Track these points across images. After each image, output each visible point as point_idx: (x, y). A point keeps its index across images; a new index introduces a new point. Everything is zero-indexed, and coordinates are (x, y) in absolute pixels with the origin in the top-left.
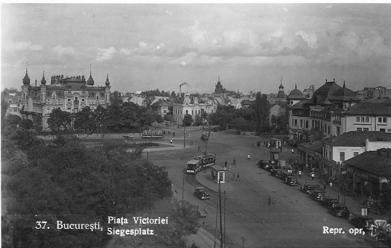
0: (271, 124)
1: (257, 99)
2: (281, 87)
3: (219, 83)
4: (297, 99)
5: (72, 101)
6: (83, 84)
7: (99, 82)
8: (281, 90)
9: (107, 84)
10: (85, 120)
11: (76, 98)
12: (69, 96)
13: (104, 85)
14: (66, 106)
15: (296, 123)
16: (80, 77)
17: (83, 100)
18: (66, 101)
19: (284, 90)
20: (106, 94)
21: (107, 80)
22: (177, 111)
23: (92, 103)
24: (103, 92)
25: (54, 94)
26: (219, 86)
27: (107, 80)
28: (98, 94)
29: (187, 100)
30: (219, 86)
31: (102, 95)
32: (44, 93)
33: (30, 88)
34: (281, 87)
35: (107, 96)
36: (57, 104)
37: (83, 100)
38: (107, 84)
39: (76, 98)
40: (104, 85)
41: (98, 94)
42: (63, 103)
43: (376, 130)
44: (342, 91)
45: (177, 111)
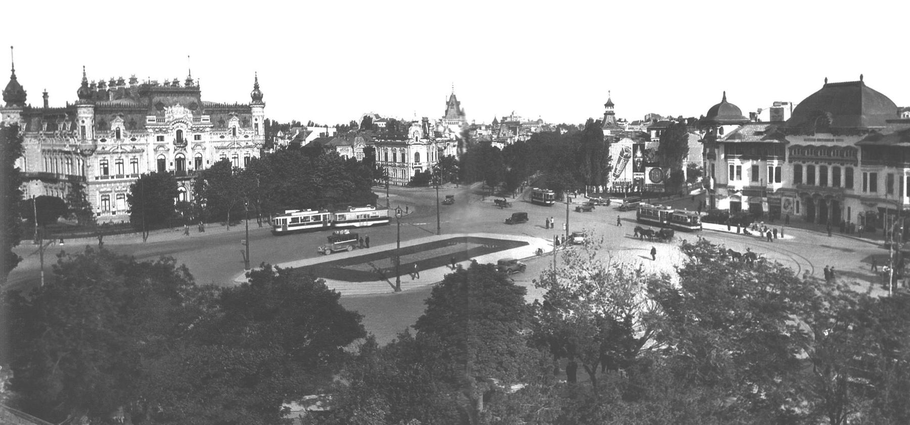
2: (609, 104)
4: (731, 124)
5: (170, 138)
6: (514, 126)
8: (609, 109)
9: (257, 97)
10: (228, 193)
11: (179, 133)
12: (161, 130)
14: (151, 152)
15: (739, 173)
16: (121, 81)
17: (198, 137)
18: (152, 139)
19: (615, 110)
20: (254, 121)
21: (256, 87)
23: (209, 149)
24: (247, 115)
25: (117, 124)
26: (453, 103)
27: (256, 87)
31: (245, 123)
32: (88, 124)
33: (28, 113)
34: (609, 104)
35: (256, 125)
36: (129, 148)
37: (198, 137)
38: (257, 97)
39: (179, 133)
40: (247, 100)
41: (234, 123)
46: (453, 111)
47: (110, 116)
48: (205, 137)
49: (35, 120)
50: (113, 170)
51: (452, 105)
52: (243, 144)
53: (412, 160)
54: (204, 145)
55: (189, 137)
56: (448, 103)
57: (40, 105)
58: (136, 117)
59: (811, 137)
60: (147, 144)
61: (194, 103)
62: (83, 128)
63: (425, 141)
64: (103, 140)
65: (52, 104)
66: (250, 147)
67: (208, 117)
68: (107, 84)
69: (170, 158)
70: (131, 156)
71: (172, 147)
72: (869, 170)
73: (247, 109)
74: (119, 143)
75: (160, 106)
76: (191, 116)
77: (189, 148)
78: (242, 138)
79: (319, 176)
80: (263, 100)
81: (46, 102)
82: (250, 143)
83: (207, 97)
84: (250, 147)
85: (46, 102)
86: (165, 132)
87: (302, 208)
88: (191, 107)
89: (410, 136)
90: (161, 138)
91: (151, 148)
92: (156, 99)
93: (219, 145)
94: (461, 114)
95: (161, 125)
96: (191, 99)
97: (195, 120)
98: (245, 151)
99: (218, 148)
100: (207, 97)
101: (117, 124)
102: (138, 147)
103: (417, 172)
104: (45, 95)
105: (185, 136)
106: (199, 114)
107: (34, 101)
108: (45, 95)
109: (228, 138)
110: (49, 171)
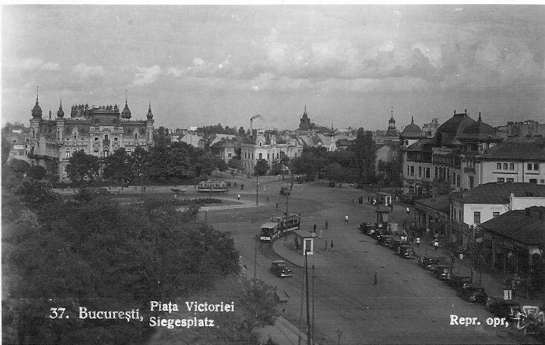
1: (358, 137)
2: (392, 121)
3: (305, 115)
4: (414, 138)
5: (101, 140)
7: (138, 115)
8: (392, 125)
9: (150, 117)
10: (118, 167)
11: (106, 136)
13: (145, 119)
14: (92, 147)
15: (412, 171)
17: (116, 139)
18: (92, 140)
21: (150, 111)
23: (127, 143)
24: (144, 127)
25: (75, 131)
26: (305, 119)
27: (150, 111)
28: (136, 131)
30: (305, 119)
31: (143, 132)
32: (61, 130)
34: (392, 121)
35: (148, 133)
36: (80, 144)
37: (116, 139)
38: (150, 117)
39: (106, 136)
40: (145, 119)
41: (136, 131)
42: (88, 144)
44: (477, 127)
49: (44, 126)
56: (301, 120)
72: (411, 164)
74: (75, 141)
87: (528, 305)
91: (92, 144)
102: (84, 144)
106: (118, 126)
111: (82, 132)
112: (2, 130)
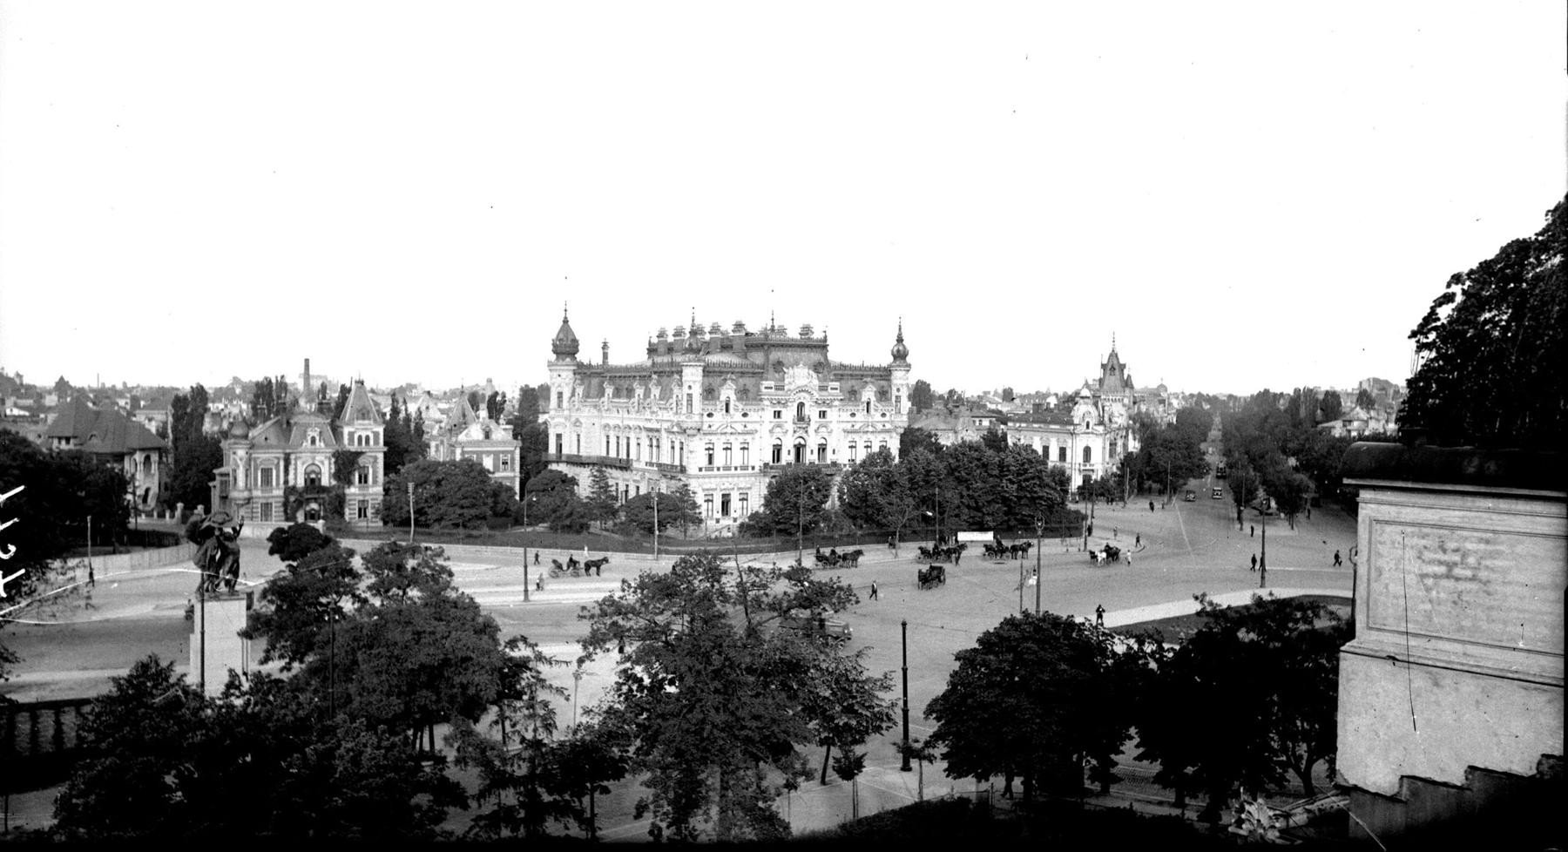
0: (730, 564)
1: (1341, 439)
3: (1114, 355)
5: (789, 414)
7: (119, 386)
9: (900, 355)
11: (801, 405)
13: (886, 360)
17: (823, 414)
18: (768, 414)
20: (894, 393)
21: (900, 340)
22: (623, 442)
25: (728, 392)
26: (1113, 366)
27: (900, 340)
28: (869, 393)
29: (925, 423)
30: (1113, 366)
31: (883, 395)
36: (740, 428)
37: (823, 414)
38: (900, 355)
39: (801, 405)
40: (886, 360)
41: (869, 393)
42: (757, 426)
43: (521, 550)
44: (960, 399)
45: (623, 442)
46: (1113, 381)
47: (719, 380)
48: (832, 414)
50: (719, 460)
51: (1113, 368)
52: (880, 427)
53: (1080, 458)
54: (831, 426)
55: (811, 412)
57: (597, 360)
58: (748, 382)
59: (475, 533)
60: (761, 423)
61: (820, 364)
62: (690, 395)
63: (1101, 429)
64: (710, 415)
65: (614, 361)
66: (888, 431)
67: (836, 384)
68: (707, 329)
69: (788, 445)
70: (741, 438)
71: (790, 426)
73: (885, 374)
75: (779, 366)
76: (816, 382)
77: (811, 429)
78: (878, 417)
79: (1012, 482)
80: (908, 359)
81: (605, 356)
82: (888, 426)
83: (835, 355)
84: (888, 431)
85: (605, 356)
86: (829, 406)
88: (818, 367)
89: (1076, 421)
90: (778, 414)
92: (776, 355)
93: (849, 426)
94: (1127, 384)
95: (780, 395)
96: (815, 356)
97: (823, 388)
98: (881, 437)
99: (847, 432)
100: (835, 355)
101: (728, 392)
102: (750, 427)
103: (1087, 479)
104: (605, 346)
105: (806, 411)
107: (589, 354)
108: (605, 346)
109: (861, 416)
110: (613, 454)
111: (743, 394)
112: (1267, 391)
